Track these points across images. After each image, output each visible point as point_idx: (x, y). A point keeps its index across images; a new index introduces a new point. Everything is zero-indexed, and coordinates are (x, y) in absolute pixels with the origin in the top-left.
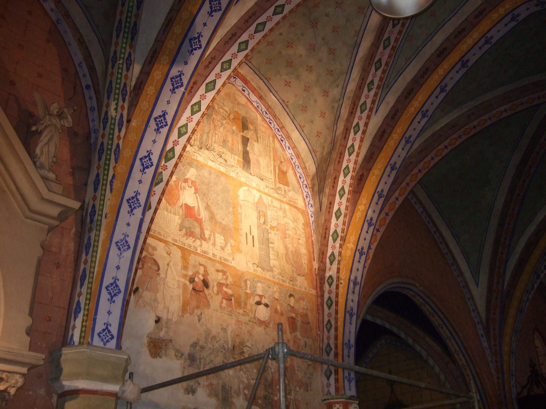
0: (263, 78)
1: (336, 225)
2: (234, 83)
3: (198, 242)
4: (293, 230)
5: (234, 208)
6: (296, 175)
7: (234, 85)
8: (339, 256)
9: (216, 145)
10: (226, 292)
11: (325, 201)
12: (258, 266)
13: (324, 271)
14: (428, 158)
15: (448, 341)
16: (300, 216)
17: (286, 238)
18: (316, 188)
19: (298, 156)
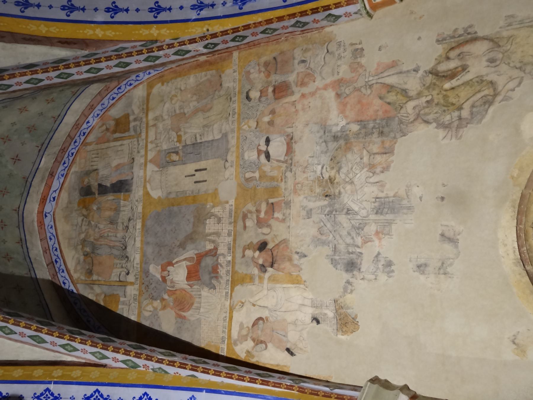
0: (28, 184)
2: (52, 213)
4: (173, 102)
5: (173, 205)
7: (54, 213)
8: (174, 47)
9: (118, 235)
10: (266, 213)
12: (227, 161)
17: (185, 114)
19: (91, 107)
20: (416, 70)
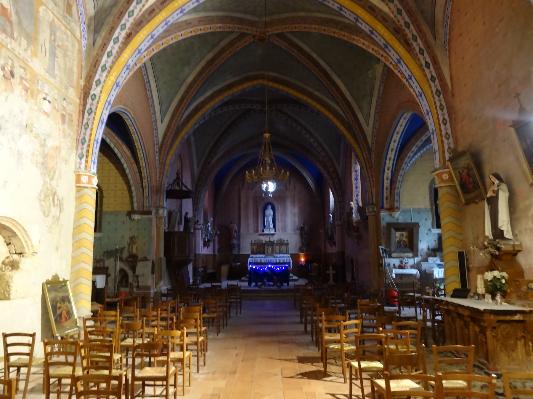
1: (107, 61)
3: (9, 40)
6: (78, 11)
11: (99, 41)
13: (90, 89)
14: (169, 38)
15: (138, 151)
16: (76, 43)
18: (92, 27)
20: (57, 186)
